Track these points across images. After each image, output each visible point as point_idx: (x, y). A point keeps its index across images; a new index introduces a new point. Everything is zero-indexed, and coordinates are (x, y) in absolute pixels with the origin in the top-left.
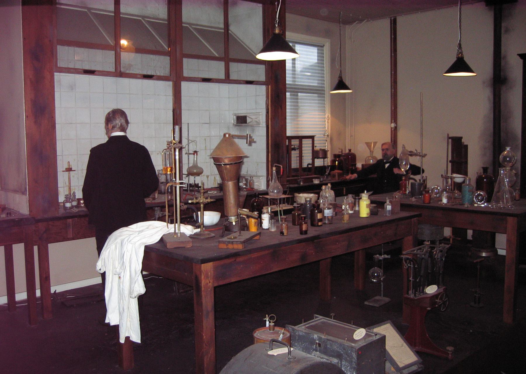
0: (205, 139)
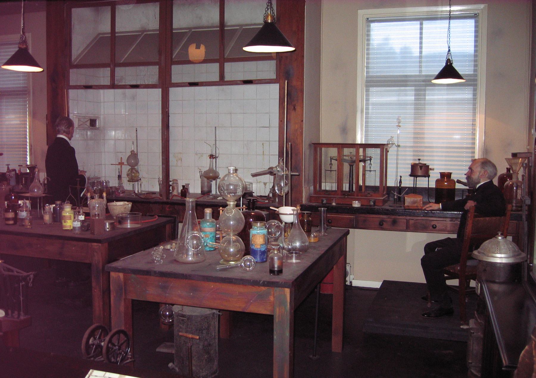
0: (263, 144)
